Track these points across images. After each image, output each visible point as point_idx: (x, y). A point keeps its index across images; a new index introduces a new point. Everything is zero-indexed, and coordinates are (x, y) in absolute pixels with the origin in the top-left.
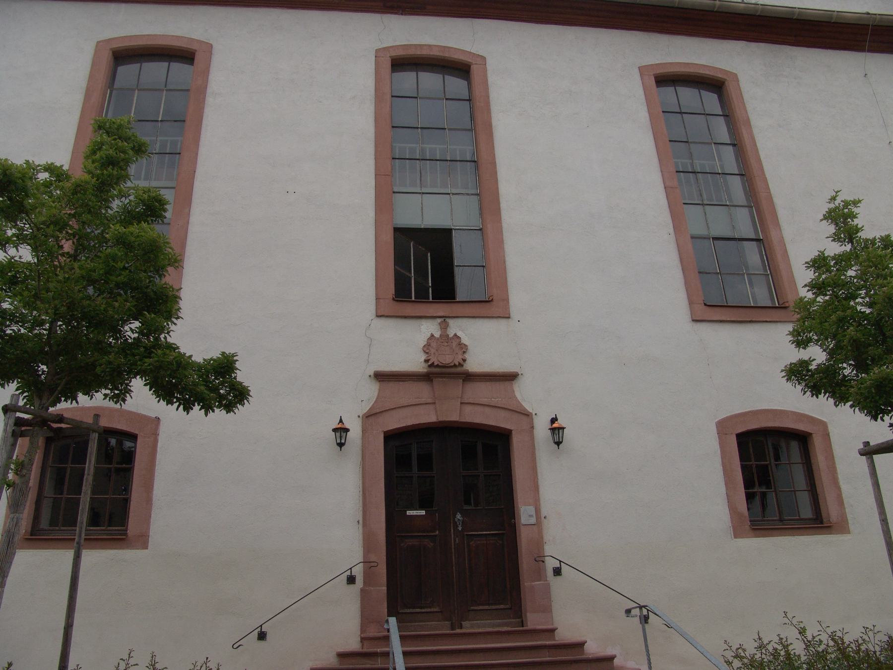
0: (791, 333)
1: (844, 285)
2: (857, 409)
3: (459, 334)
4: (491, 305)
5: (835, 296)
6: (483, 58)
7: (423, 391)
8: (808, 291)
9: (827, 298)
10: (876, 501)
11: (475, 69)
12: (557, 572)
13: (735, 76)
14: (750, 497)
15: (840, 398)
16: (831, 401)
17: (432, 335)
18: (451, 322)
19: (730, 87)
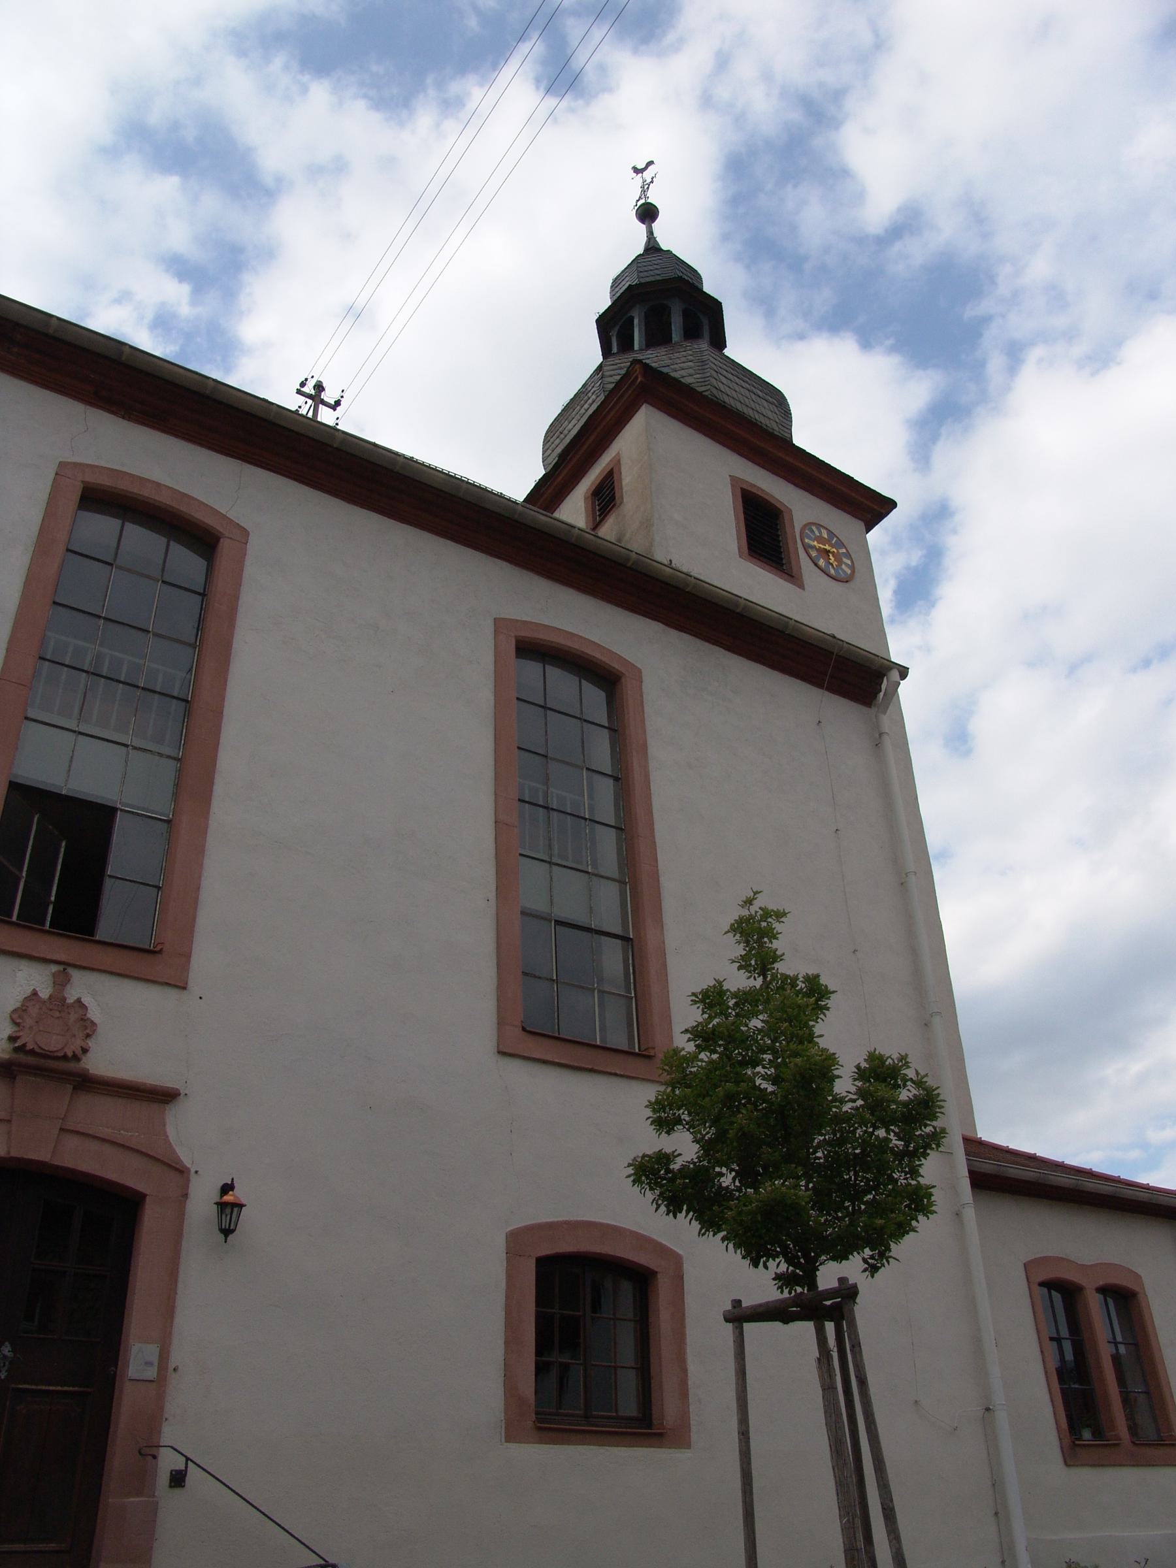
0: (650, 1105)
1: (744, 1041)
2: (731, 1246)
3: (86, 1000)
4: (157, 958)
5: (727, 1055)
6: (245, 533)
8: (689, 1040)
9: (715, 1056)
10: (738, 1399)
11: (225, 546)
12: (178, 1479)
13: (638, 674)
14: (541, 1369)
15: (709, 1223)
16: (696, 1225)
17: (35, 993)
18: (76, 975)
19: (628, 685)
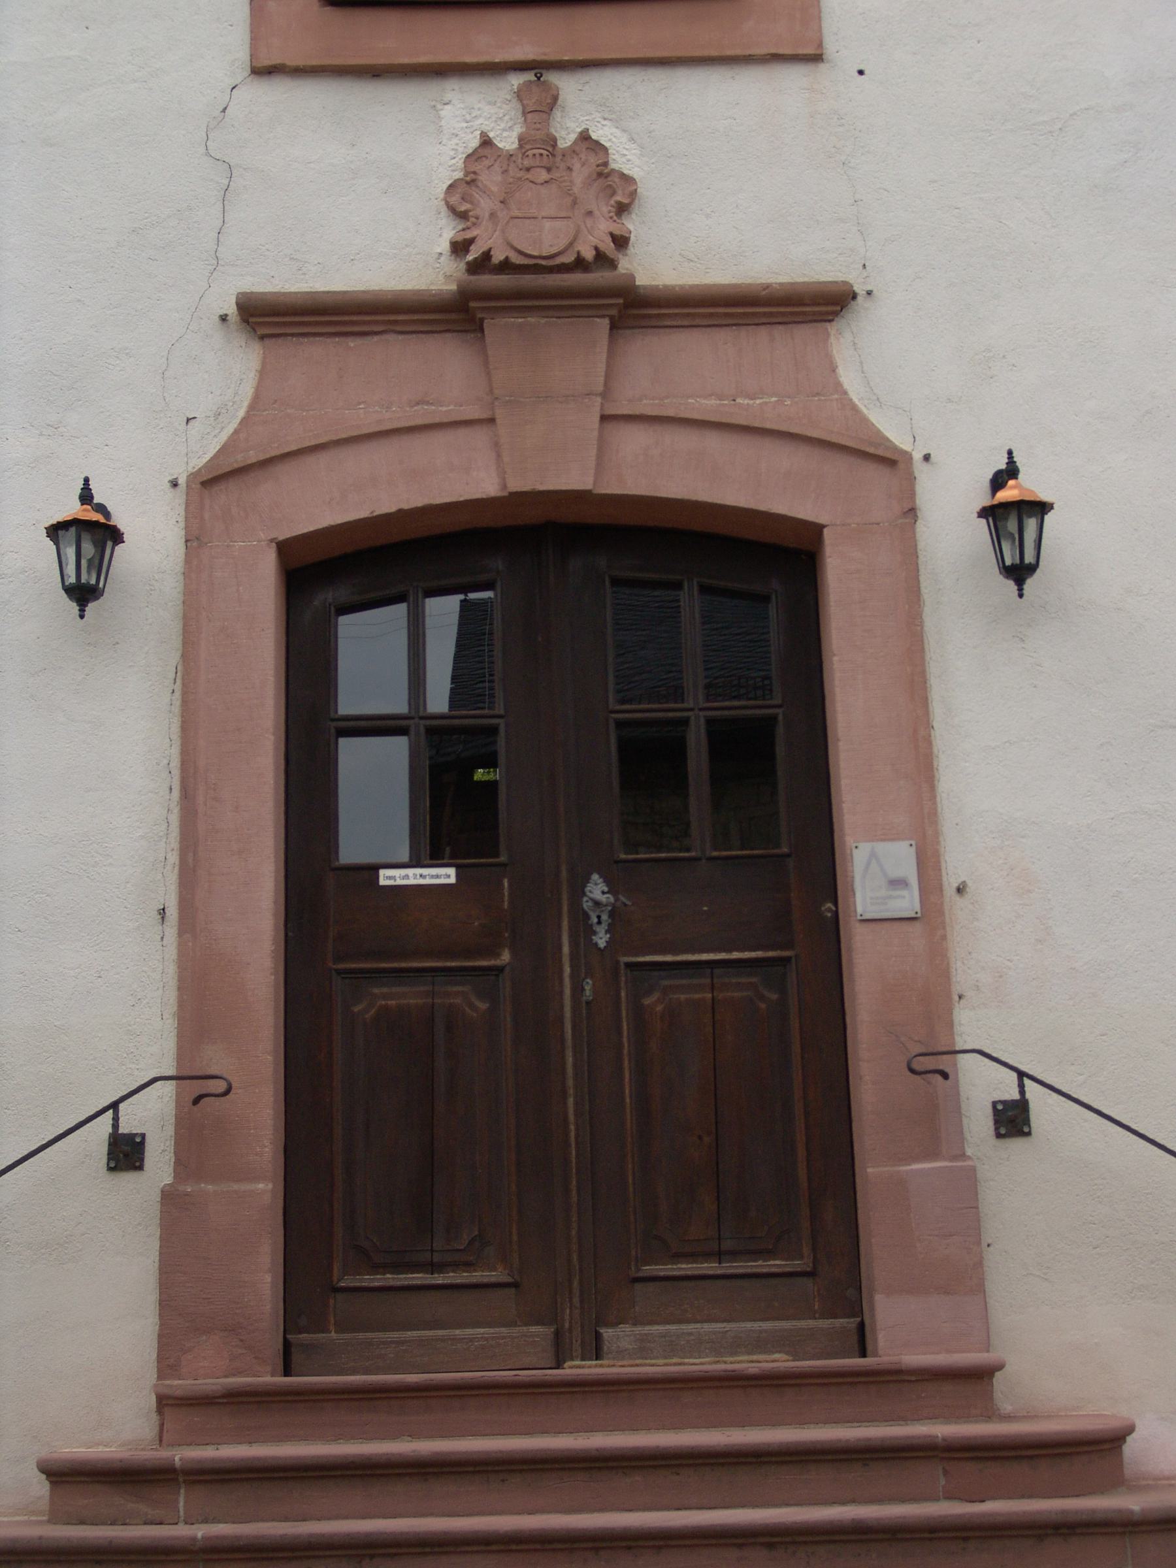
7: (444, 373)
12: (1012, 1120)
17: (486, 142)
18: (568, 85)
